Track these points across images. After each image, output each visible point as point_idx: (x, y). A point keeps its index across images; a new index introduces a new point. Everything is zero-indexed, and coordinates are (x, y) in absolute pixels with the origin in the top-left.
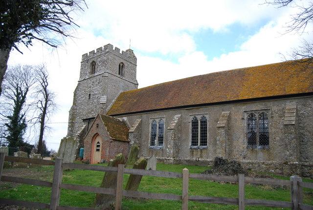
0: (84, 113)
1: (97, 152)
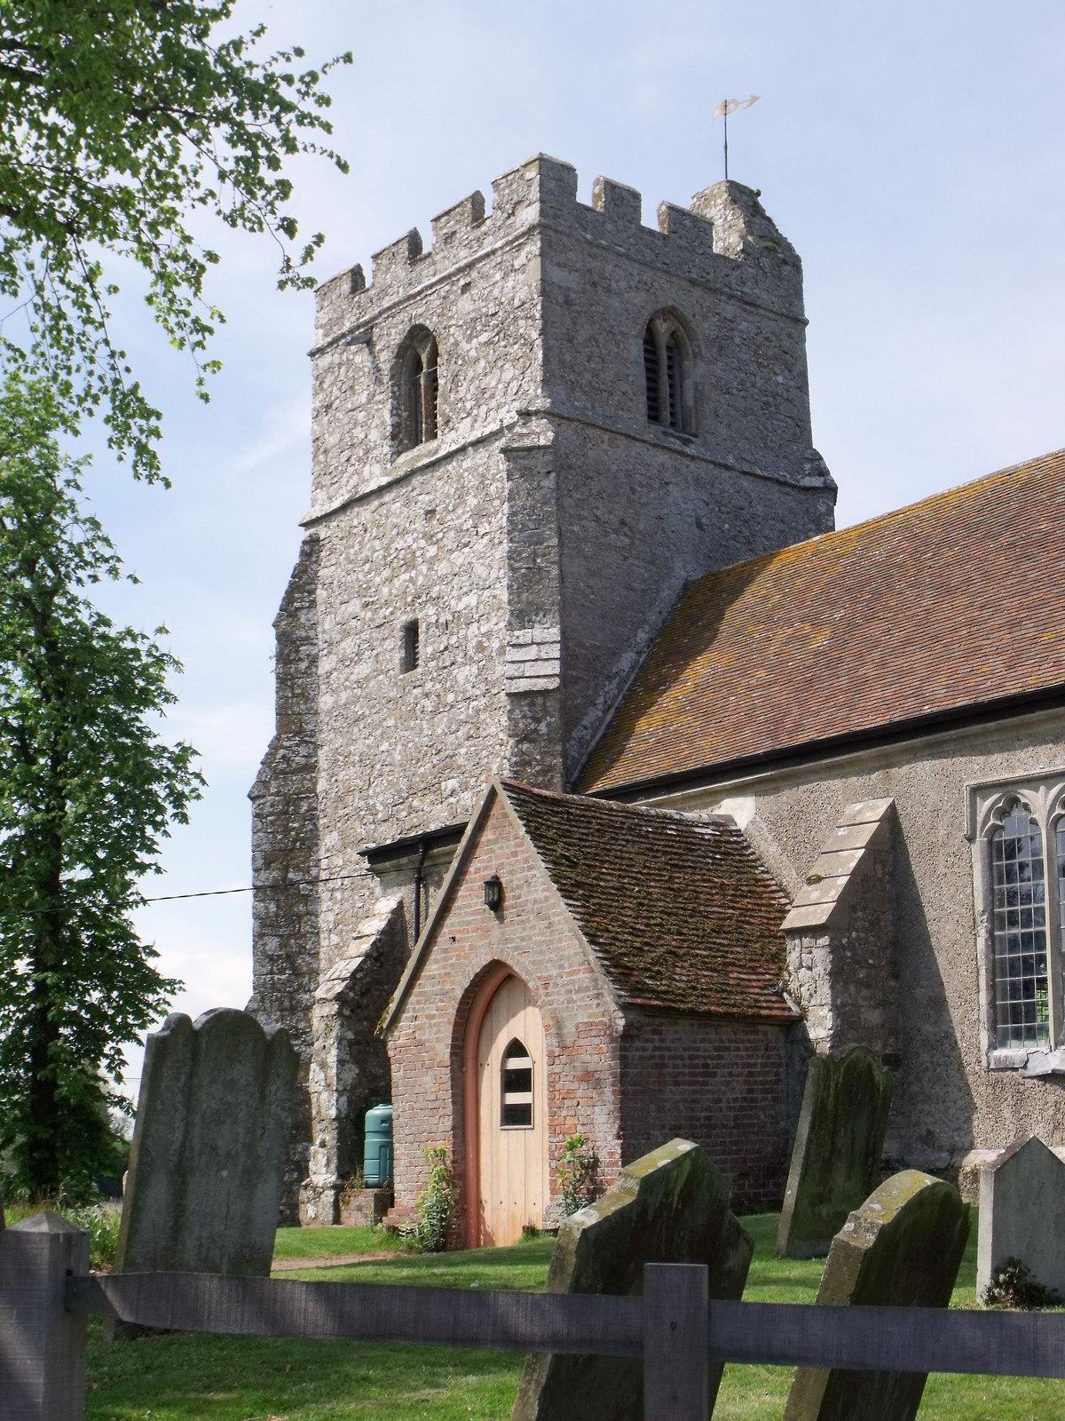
0: (380, 797)
1: (516, 1136)
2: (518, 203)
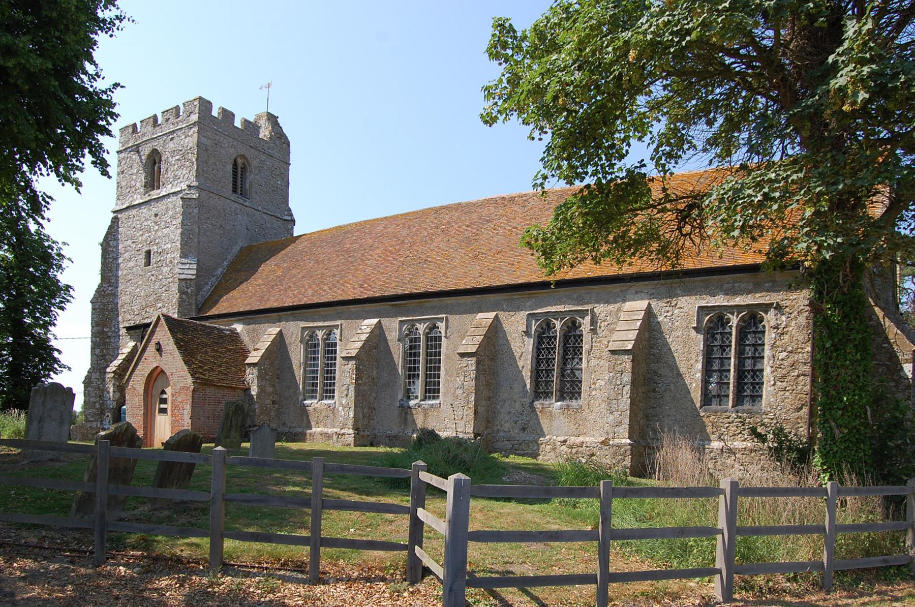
0: (136, 308)
2: (191, 113)
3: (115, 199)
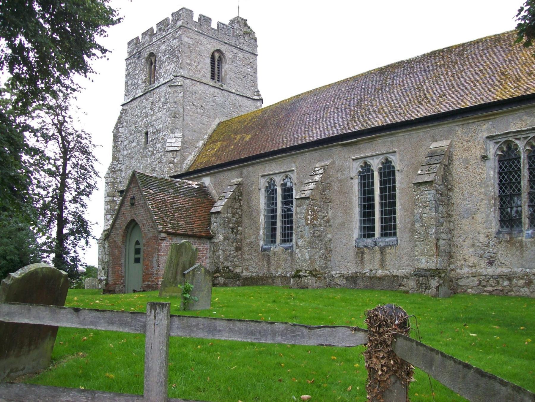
2: (178, 20)
3: (124, 96)
